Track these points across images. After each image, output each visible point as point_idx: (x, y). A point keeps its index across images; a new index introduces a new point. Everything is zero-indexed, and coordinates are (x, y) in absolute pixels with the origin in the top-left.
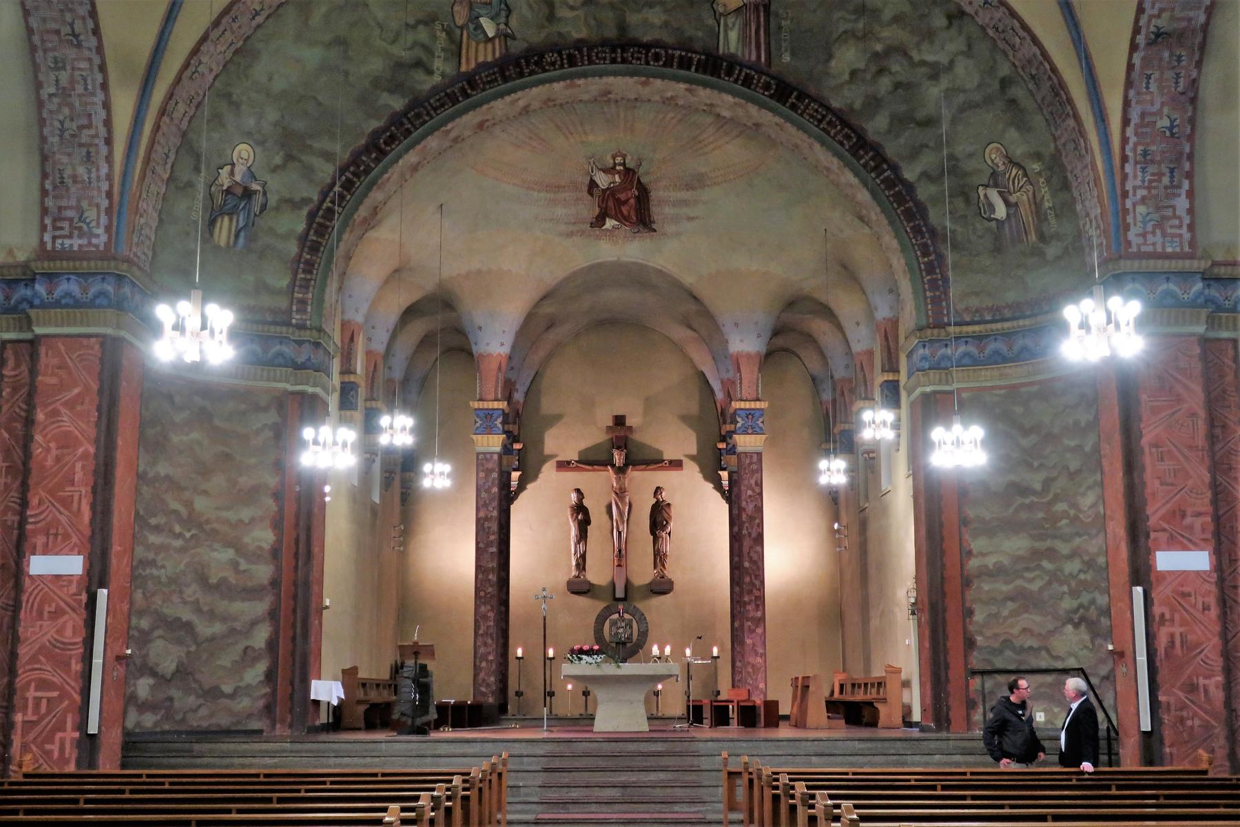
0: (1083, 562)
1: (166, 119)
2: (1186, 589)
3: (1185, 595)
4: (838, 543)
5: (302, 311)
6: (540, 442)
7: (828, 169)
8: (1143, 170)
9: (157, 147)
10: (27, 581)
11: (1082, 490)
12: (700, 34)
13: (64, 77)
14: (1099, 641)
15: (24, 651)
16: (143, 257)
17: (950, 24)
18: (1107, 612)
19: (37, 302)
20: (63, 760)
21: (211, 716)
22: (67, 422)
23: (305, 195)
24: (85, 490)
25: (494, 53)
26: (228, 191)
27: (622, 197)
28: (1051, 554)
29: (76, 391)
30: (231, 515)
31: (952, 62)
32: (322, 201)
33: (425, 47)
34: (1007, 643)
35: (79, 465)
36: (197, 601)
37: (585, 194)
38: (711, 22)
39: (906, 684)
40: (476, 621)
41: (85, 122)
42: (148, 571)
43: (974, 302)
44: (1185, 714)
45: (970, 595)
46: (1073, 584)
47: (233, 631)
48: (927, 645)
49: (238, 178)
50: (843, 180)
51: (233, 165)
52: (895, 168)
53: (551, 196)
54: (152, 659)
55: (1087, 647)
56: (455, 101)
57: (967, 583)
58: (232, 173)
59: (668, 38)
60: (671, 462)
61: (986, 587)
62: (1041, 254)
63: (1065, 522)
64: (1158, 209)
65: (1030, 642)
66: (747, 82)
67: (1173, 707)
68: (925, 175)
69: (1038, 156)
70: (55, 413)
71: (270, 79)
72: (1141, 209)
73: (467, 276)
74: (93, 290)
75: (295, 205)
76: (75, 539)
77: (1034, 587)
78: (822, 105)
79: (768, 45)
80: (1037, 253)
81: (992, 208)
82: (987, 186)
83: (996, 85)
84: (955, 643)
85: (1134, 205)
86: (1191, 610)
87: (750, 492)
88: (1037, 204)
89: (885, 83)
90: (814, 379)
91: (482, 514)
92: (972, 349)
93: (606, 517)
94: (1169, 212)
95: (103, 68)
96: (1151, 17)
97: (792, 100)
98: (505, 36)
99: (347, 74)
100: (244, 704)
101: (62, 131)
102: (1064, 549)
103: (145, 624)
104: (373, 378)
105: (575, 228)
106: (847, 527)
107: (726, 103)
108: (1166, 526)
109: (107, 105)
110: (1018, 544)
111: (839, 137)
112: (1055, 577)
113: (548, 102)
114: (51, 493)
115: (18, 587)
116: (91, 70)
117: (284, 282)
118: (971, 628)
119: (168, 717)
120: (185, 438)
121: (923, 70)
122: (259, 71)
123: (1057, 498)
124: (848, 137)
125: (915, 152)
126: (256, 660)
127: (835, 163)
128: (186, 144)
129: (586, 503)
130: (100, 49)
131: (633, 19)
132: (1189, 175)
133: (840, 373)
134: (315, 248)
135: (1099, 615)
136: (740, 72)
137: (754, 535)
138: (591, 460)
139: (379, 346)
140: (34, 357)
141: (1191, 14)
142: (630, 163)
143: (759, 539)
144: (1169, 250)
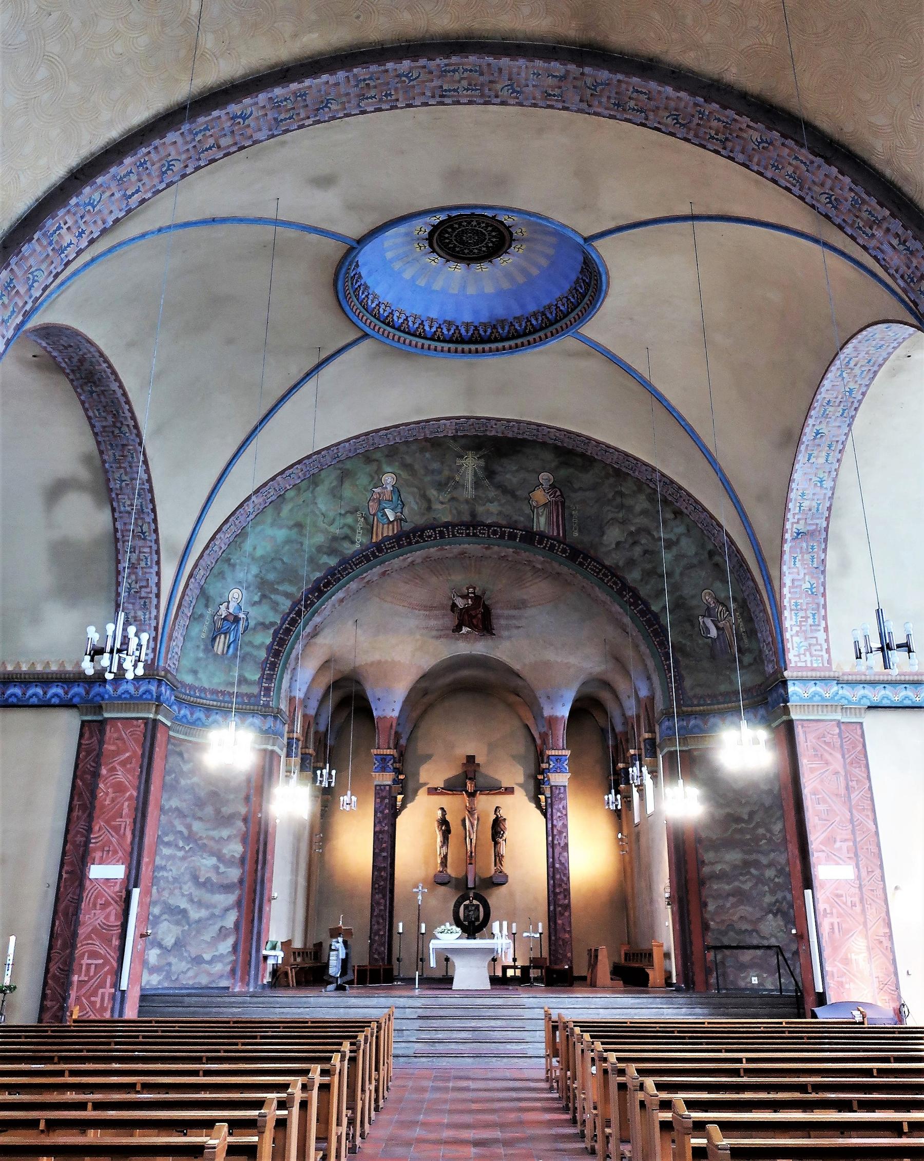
0: (777, 870)
1: (192, 580)
2: (839, 892)
3: (840, 896)
4: (622, 848)
5: (267, 694)
6: (417, 774)
7: (604, 602)
9: (186, 598)
10: (88, 883)
11: (773, 820)
12: (522, 519)
13: (134, 556)
14: (789, 926)
15: (82, 931)
16: (173, 666)
17: (676, 518)
19: (106, 696)
20: (103, 1009)
22: (121, 776)
23: (272, 620)
24: (129, 821)
26: (225, 619)
27: (473, 613)
28: (756, 864)
29: (127, 755)
30: (215, 834)
31: (678, 540)
33: (350, 527)
34: (731, 927)
35: (126, 804)
36: (191, 894)
37: (449, 612)
38: (527, 511)
39: (667, 955)
40: (372, 906)
41: (144, 584)
42: (161, 874)
43: (699, 691)
44: (843, 979)
45: (705, 892)
47: (213, 916)
49: (231, 610)
50: (613, 609)
51: (229, 602)
52: (646, 603)
53: (427, 613)
54: (159, 937)
55: (782, 931)
56: (369, 560)
57: (702, 883)
58: (228, 608)
59: (504, 523)
60: (506, 789)
61: (715, 887)
63: (764, 841)
64: (806, 639)
65: (745, 926)
67: (836, 976)
70: (113, 769)
71: (255, 548)
72: (796, 639)
73: (372, 664)
74: (142, 689)
75: (264, 626)
76: (120, 854)
77: (747, 887)
78: (598, 563)
82: (704, 616)
83: (706, 555)
84: (696, 927)
85: (792, 636)
86: (843, 906)
87: (559, 814)
89: (638, 550)
91: (377, 829)
93: (462, 828)
94: (814, 641)
95: (158, 552)
96: (793, 524)
98: (399, 520)
99: (302, 544)
100: (218, 968)
101: (130, 589)
102: (764, 861)
103: (156, 910)
104: (307, 733)
105: (442, 633)
107: (539, 559)
108: (824, 848)
109: (158, 574)
110: (734, 856)
112: (760, 880)
113: (427, 558)
114: (107, 822)
115: (81, 886)
116: (151, 553)
117: (257, 677)
118: (707, 916)
119: (168, 977)
120: (189, 782)
122: (248, 546)
123: (758, 826)
124: (615, 583)
126: (226, 937)
127: (608, 599)
128: (203, 592)
129: (448, 818)
130: (157, 541)
131: (480, 509)
132: (825, 618)
133: (619, 728)
134: (277, 654)
135: (788, 908)
136: (547, 541)
137: (562, 845)
138: (452, 787)
139: (312, 712)
140: (102, 732)
141: (818, 521)
144: (815, 665)
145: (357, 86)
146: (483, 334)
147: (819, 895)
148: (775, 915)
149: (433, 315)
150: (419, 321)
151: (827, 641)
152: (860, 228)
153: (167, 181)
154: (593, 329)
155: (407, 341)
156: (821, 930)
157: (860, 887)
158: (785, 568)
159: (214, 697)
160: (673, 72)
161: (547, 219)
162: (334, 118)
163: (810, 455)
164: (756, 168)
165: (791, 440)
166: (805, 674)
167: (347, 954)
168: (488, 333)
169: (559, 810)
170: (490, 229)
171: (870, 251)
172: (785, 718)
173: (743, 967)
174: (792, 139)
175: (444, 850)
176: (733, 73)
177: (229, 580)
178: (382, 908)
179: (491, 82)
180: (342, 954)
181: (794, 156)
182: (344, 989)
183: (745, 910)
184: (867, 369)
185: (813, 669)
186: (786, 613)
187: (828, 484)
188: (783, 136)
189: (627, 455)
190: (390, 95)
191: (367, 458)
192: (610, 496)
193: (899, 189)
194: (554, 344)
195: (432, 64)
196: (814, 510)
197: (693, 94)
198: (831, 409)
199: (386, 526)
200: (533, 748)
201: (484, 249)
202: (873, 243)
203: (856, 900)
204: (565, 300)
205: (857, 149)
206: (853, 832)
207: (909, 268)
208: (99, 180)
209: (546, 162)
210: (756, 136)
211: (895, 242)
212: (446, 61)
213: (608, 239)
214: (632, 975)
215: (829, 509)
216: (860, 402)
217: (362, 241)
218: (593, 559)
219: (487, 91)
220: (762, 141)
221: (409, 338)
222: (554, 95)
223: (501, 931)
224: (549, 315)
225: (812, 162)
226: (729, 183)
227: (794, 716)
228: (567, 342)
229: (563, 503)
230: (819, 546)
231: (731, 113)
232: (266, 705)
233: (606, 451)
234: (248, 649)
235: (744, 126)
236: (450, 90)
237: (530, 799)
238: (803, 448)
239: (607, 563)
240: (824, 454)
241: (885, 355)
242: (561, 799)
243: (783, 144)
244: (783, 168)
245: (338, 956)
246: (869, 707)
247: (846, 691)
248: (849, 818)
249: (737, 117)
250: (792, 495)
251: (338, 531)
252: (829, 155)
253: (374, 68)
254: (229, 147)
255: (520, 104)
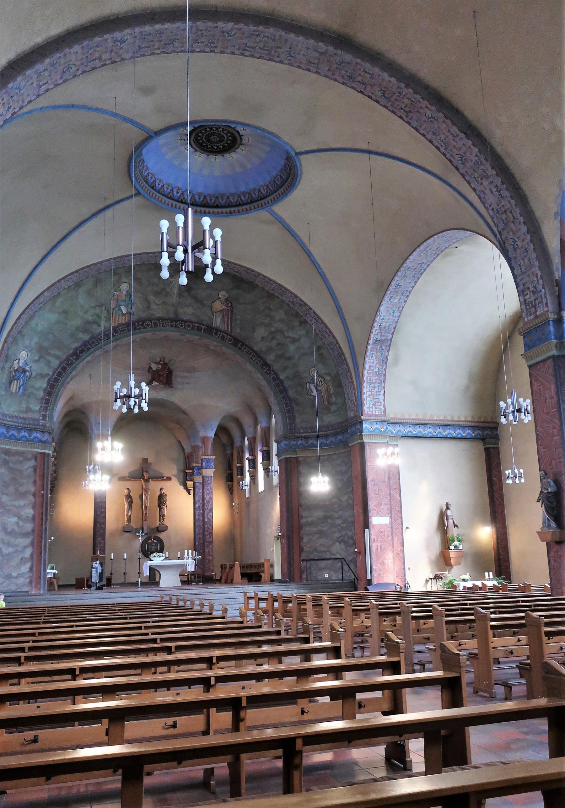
2: (381, 530)
3: (381, 532)
8: (370, 386)
12: (206, 318)
17: (301, 325)
18: (351, 538)
21: (8, 586)
25: (125, 319)
26: (17, 370)
27: (161, 373)
28: (331, 517)
32: (53, 375)
34: (315, 550)
36: (3, 539)
38: (210, 314)
43: (304, 425)
44: (381, 572)
45: (302, 532)
46: (339, 528)
47: (16, 551)
48: (285, 550)
49: (21, 365)
58: (19, 363)
59: (194, 320)
60: (167, 477)
62: (329, 409)
63: (336, 506)
64: (374, 399)
65: (323, 549)
66: (223, 338)
68: (287, 377)
69: (329, 374)
72: (368, 399)
75: (42, 376)
77: (325, 529)
78: (250, 348)
79: (231, 325)
80: (327, 408)
81: (311, 391)
87: (208, 492)
88: (328, 390)
89: (275, 342)
90: (224, 445)
92: (303, 442)
94: (377, 400)
96: (375, 335)
97: (239, 346)
99: (66, 324)
100: (21, 580)
106: (238, 504)
111: (256, 361)
117: (37, 408)
121: (289, 339)
122: (33, 324)
124: (259, 361)
125: (285, 369)
126: (25, 563)
129: (131, 494)
131: (181, 311)
132: (384, 388)
141: (387, 334)
142: (166, 361)
143: (211, 510)
144: (377, 413)
145: (195, 33)
146: (209, 201)
147: (372, 532)
148: (340, 543)
149: (180, 186)
150: (170, 188)
151: (384, 400)
152: (475, 178)
153: (64, 78)
154: (278, 208)
155: (163, 201)
156: (372, 549)
157: (392, 527)
158: (367, 359)
159: (11, 420)
160: (389, 64)
161: (278, 137)
162: (174, 52)
163: (391, 297)
164: (422, 132)
165: (382, 288)
166: (372, 418)
167: (102, 570)
168: (213, 201)
169: (208, 490)
170: (229, 134)
171: (477, 192)
172: (360, 441)
173: (320, 569)
174: (450, 120)
175: (129, 513)
176: (427, 73)
177: (20, 345)
178: (103, 545)
179: (278, 47)
180: (100, 570)
181: (447, 129)
182: (102, 589)
183: (323, 541)
184: (435, 252)
185: (376, 416)
186: (365, 384)
187: (397, 314)
188: (446, 117)
189: (281, 286)
190: (214, 43)
191: (115, 273)
192: (262, 309)
193: (502, 160)
194: (254, 214)
195: (246, 29)
196: (387, 328)
197: (399, 80)
198: (409, 272)
199: (120, 317)
200: (182, 454)
201: (221, 147)
202: (479, 188)
203: (389, 533)
204: (265, 187)
205: (484, 133)
206: (390, 500)
207: (498, 205)
208: (28, 72)
209: (281, 99)
210: (428, 113)
211: (494, 190)
212: (255, 28)
213: (310, 155)
214: (253, 575)
215: (395, 328)
216: (425, 270)
217: (158, 133)
218: (247, 346)
219: (273, 52)
220: (432, 117)
221: (164, 198)
222: (313, 63)
223: (188, 555)
224: (253, 195)
225: (458, 135)
226: (399, 135)
227: (365, 440)
228: (263, 214)
229: (232, 311)
230: (386, 349)
231: (418, 97)
232: (44, 426)
233: (268, 283)
234: (31, 390)
235: (423, 106)
236: (251, 47)
237: (180, 484)
238: (388, 292)
239: (255, 349)
240: (398, 297)
241: (447, 245)
242: (209, 484)
243: (444, 122)
244: (439, 135)
245: (97, 571)
246: (402, 436)
247: (391, 428)
248: (389, 493)
249: (421, 100)
250: (377, 319)
251: (90, 318)
252: (468, 132)
253: (210, 24)
254: (106, 60)
255: (291, 65)
